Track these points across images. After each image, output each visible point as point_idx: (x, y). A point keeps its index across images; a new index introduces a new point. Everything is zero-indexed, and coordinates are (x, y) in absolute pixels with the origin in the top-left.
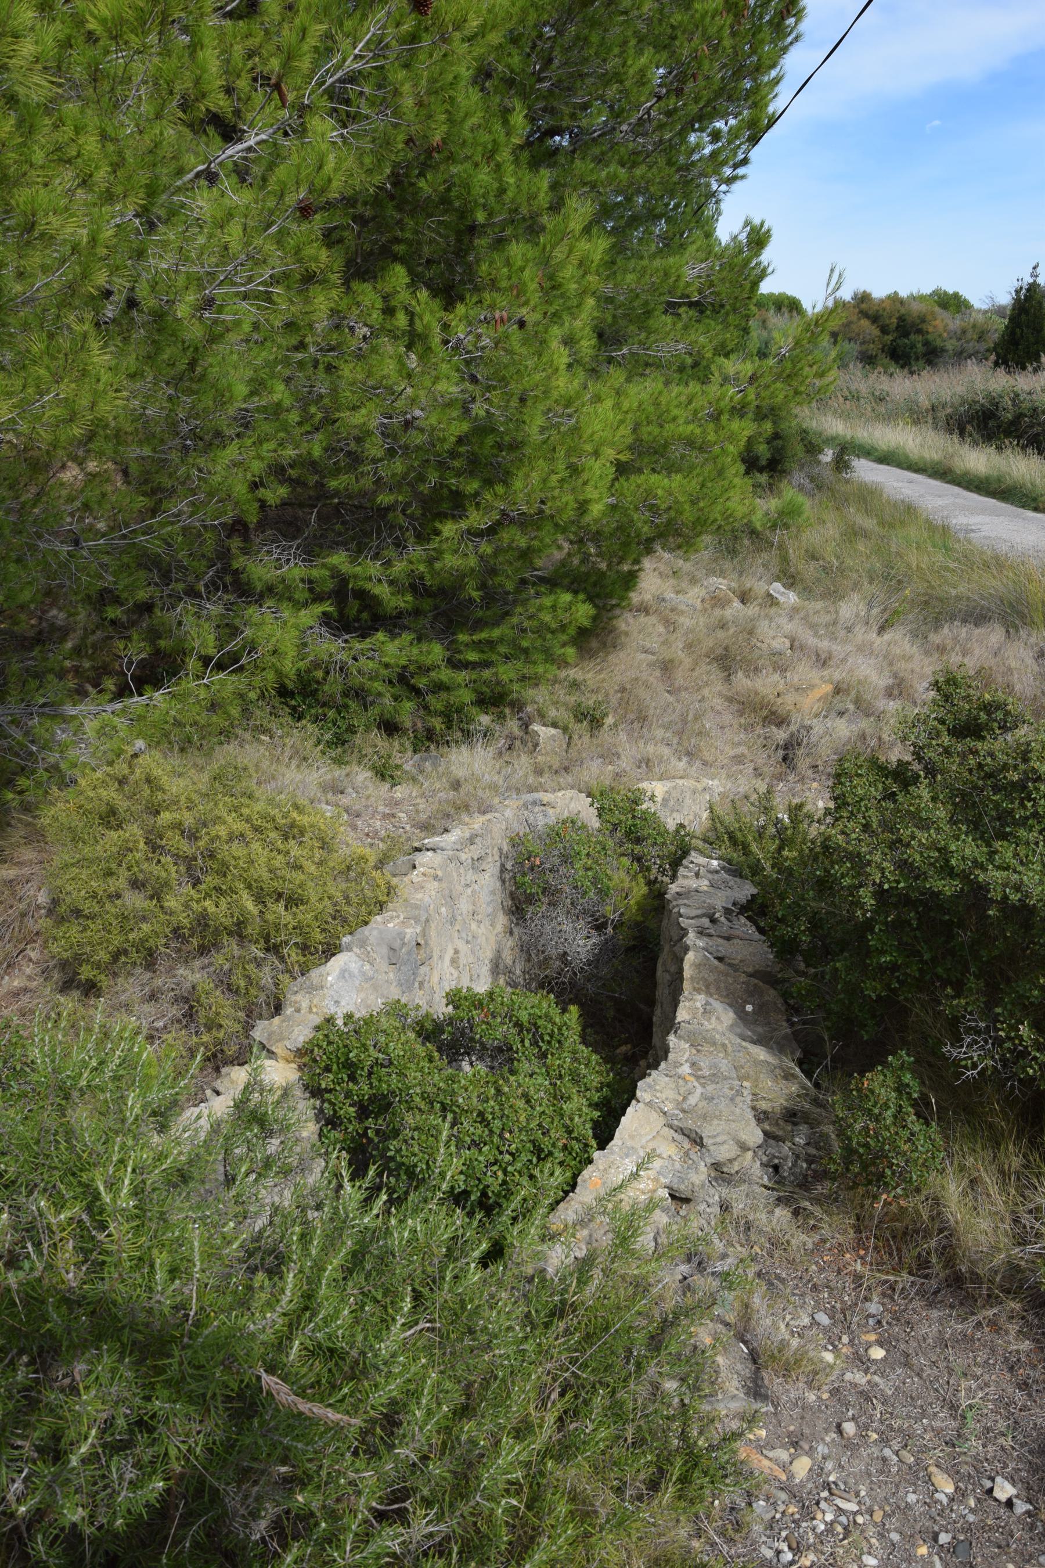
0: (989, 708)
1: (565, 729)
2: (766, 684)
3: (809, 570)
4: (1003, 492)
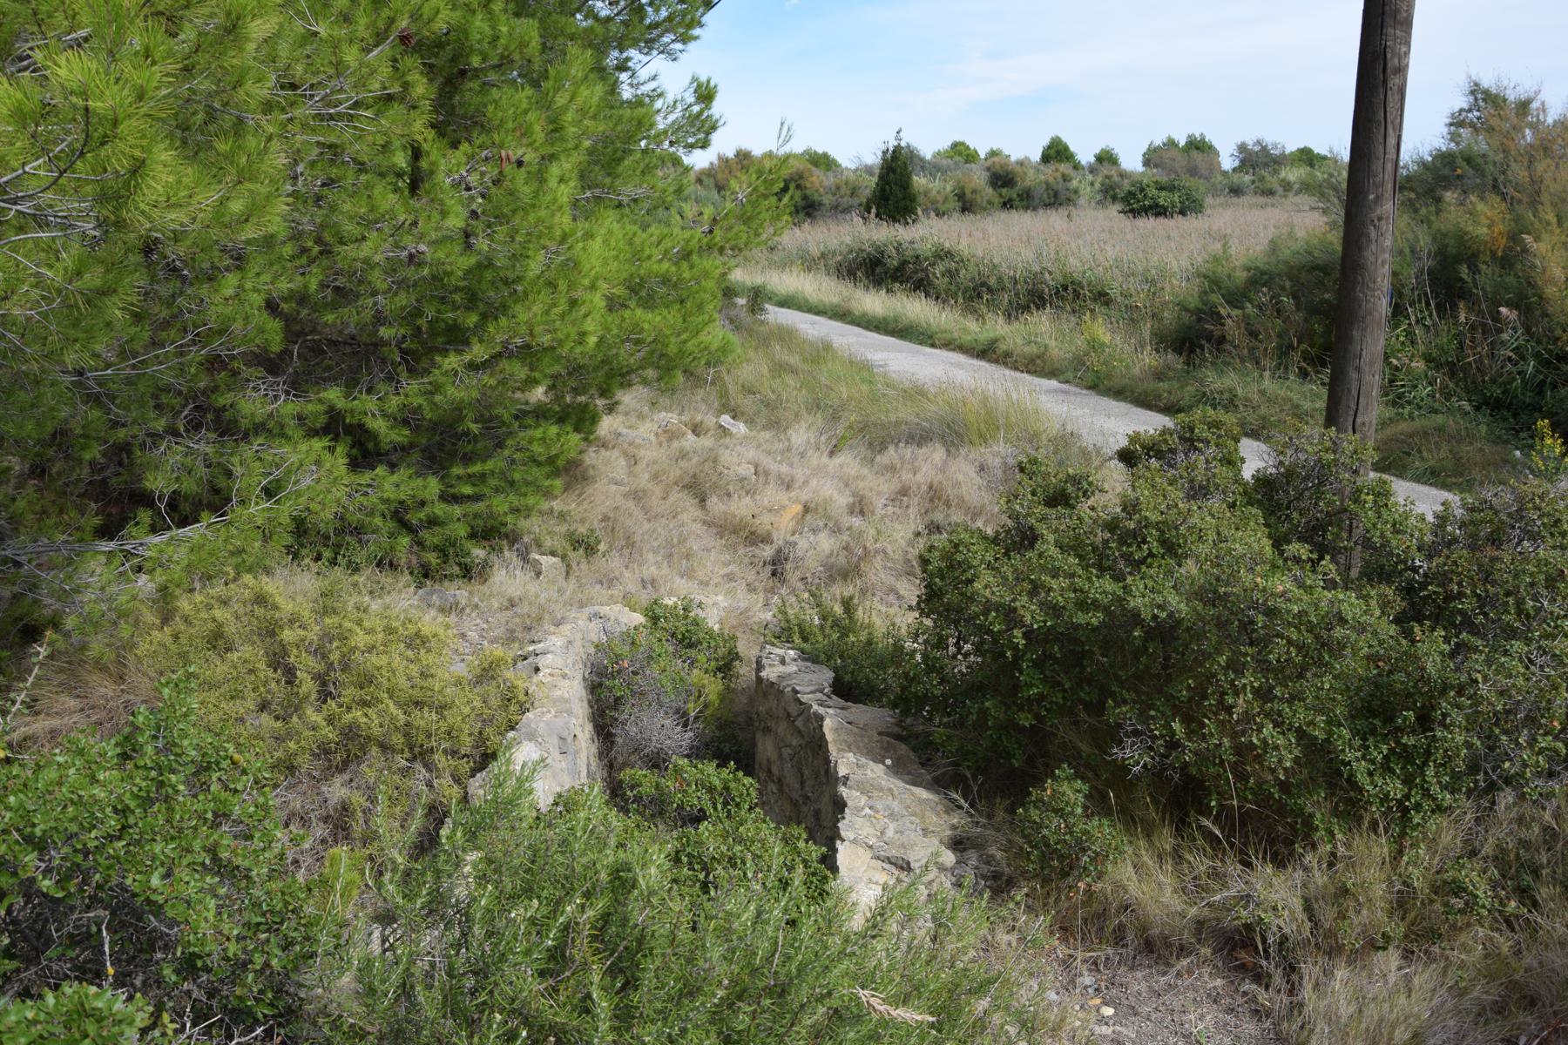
0: (1075, 480)
1: (564, 557)
2: (741, 507)
3: (747, 403)
4: (901, 331)
